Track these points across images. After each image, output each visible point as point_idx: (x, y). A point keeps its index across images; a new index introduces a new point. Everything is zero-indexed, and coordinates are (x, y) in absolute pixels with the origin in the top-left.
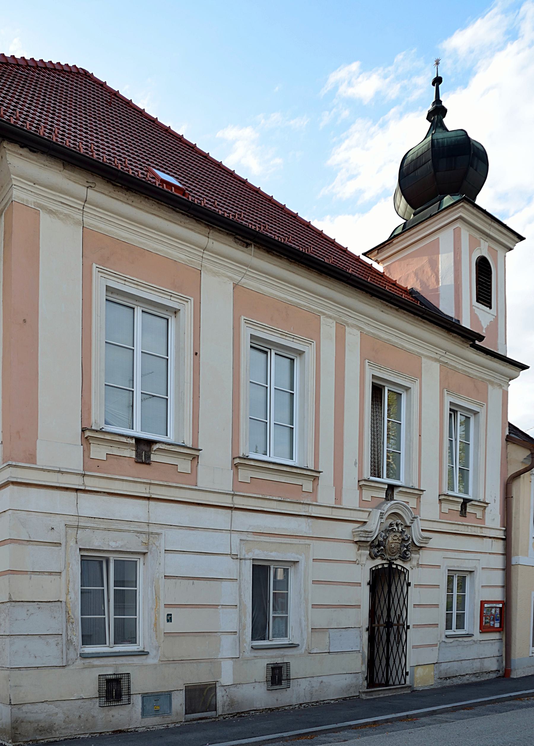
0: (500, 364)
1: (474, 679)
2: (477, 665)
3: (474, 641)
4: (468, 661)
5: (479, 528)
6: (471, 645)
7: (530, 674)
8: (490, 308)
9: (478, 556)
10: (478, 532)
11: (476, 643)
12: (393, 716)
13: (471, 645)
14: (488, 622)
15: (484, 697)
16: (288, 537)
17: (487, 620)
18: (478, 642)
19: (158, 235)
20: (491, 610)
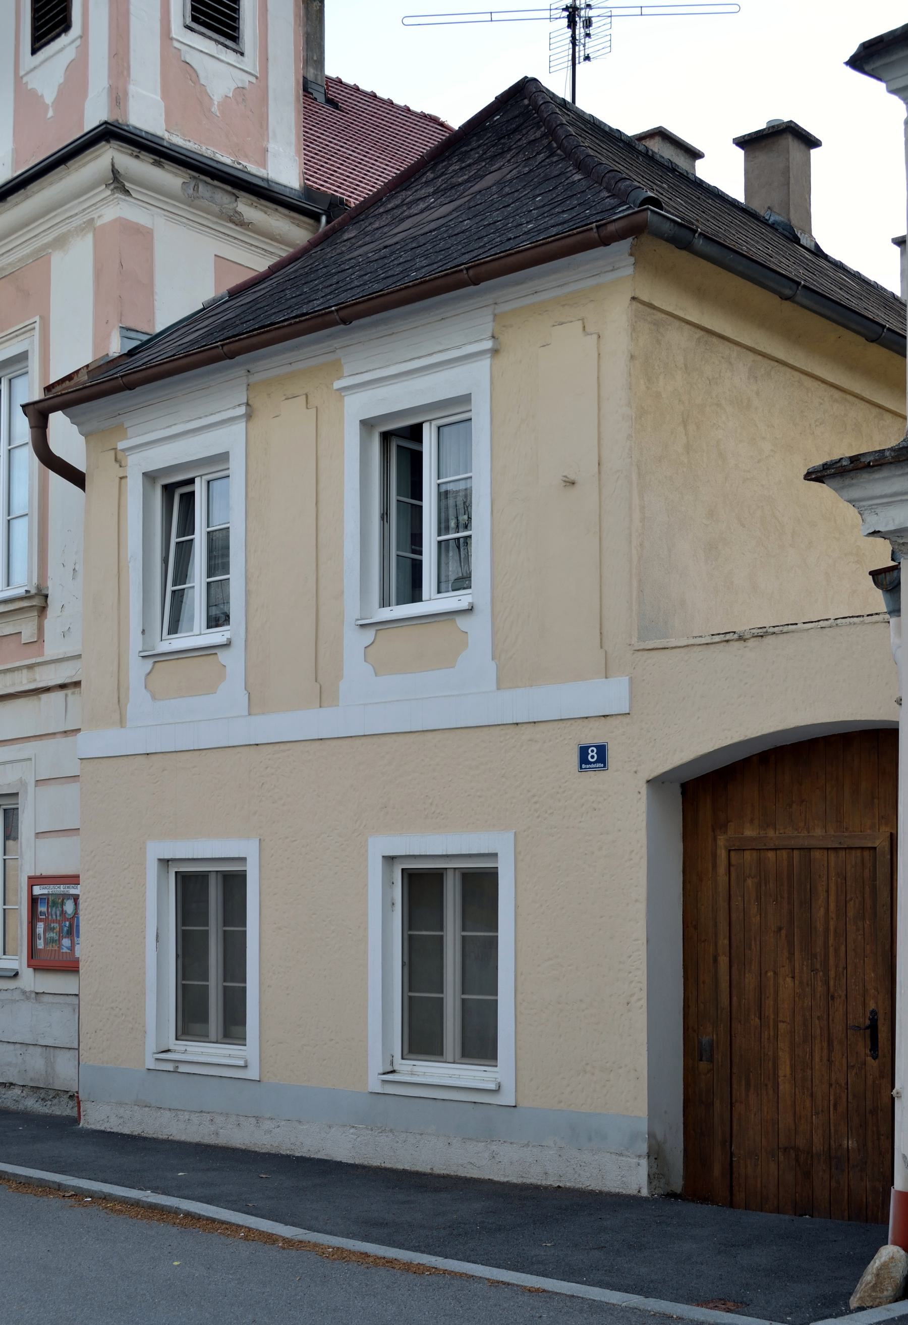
0: (51, 184)
1: (31, 1104)
2: (36, 1063)
3: (24, 992)
4: (11, 1047)
5: (25, 671)
6: (14, 1001)
7: (126, 1131)
8: (34, 52)
9: (27, 750)
10: (23, 682)
11: (28, 998)
12: (107, 1188)
13: (14, 1001)
14: (53, 941)
15: (401, 1246)
16: (10, 743)
17: (52, 935)
18: (33, 995)
19: (89, 198)
20: (63, 904)
